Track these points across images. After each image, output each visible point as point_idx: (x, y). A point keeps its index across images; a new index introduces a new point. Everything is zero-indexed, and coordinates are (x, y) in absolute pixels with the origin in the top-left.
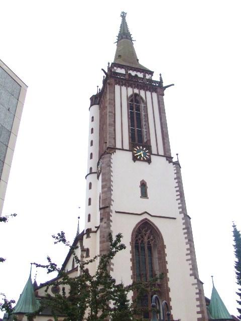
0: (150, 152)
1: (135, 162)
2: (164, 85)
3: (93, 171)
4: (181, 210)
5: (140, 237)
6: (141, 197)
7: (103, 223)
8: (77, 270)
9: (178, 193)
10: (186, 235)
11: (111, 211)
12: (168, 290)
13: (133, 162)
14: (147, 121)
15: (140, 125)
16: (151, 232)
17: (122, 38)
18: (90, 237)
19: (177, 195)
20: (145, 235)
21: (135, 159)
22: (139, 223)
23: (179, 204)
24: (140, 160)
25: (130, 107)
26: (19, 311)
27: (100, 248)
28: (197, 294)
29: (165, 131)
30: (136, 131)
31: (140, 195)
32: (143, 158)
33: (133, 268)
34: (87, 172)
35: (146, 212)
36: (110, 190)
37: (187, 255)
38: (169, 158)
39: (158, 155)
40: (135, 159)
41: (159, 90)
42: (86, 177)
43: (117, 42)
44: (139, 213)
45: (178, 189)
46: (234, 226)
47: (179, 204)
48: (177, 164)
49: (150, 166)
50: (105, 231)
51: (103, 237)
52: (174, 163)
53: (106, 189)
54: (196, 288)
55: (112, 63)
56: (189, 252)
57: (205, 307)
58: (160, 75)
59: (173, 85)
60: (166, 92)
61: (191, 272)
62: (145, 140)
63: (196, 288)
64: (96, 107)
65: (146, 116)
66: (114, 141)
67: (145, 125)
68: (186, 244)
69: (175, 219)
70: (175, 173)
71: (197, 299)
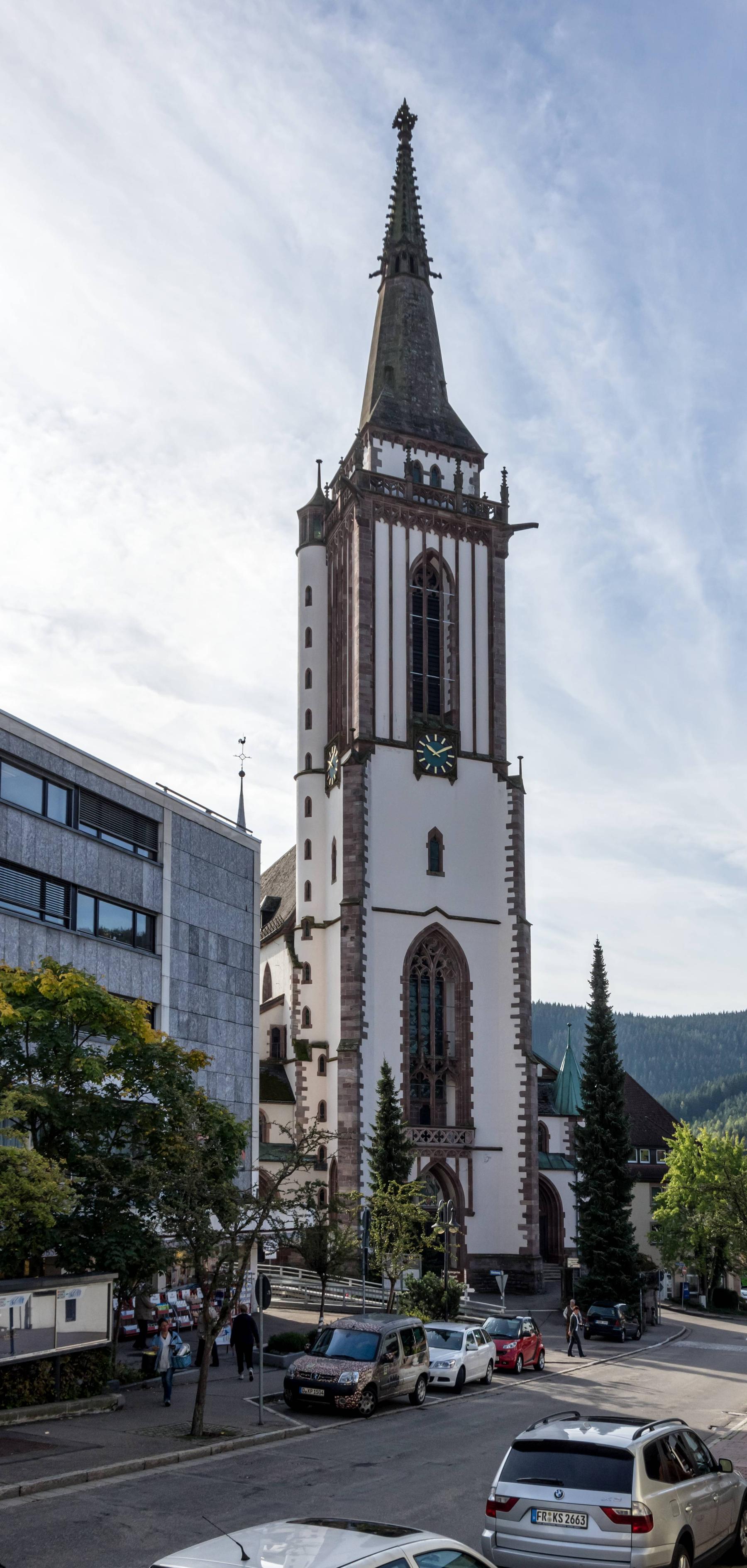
0: (457, 752)
1: (418, 778)
2: (512, 520)
4: (512, 906)
9: (511, 864)
10: (516, 965)
14: (455, 649)
15: (435, 666)
16: (445, 950)
19: (508, 869)
20: (432, 957)
21: (419, 770)
22: (420, 934)
23: (510, 890)
24: (430, 773)
25: (415, 602)
27: (342, 1012)
28: (522, 1083)
29: (497, 683)
33: (404, 1031)
35: (436, 909)
36: (363, 859)
37: (514, 1005)
38: (499, 765)
40: (419, 770)
43: (381, 272)
45: (511, 853)
47: (510, 890)
48: (516, 785)
50: (353, 957)
51: (349, 970)
54: (523, 1074)
56: (517, 1000)
57: (535, 1137)
58: (504, 473)
59: (536, 525)
60: (515, 543)
61: (515, 944)
62: (447, 708)
63: (523, 1074)
65: (455, 630)
66: (371, 717)
67: (449, 660)
68: (515, 983)
70: (510, 812)
71: (522, 1094)
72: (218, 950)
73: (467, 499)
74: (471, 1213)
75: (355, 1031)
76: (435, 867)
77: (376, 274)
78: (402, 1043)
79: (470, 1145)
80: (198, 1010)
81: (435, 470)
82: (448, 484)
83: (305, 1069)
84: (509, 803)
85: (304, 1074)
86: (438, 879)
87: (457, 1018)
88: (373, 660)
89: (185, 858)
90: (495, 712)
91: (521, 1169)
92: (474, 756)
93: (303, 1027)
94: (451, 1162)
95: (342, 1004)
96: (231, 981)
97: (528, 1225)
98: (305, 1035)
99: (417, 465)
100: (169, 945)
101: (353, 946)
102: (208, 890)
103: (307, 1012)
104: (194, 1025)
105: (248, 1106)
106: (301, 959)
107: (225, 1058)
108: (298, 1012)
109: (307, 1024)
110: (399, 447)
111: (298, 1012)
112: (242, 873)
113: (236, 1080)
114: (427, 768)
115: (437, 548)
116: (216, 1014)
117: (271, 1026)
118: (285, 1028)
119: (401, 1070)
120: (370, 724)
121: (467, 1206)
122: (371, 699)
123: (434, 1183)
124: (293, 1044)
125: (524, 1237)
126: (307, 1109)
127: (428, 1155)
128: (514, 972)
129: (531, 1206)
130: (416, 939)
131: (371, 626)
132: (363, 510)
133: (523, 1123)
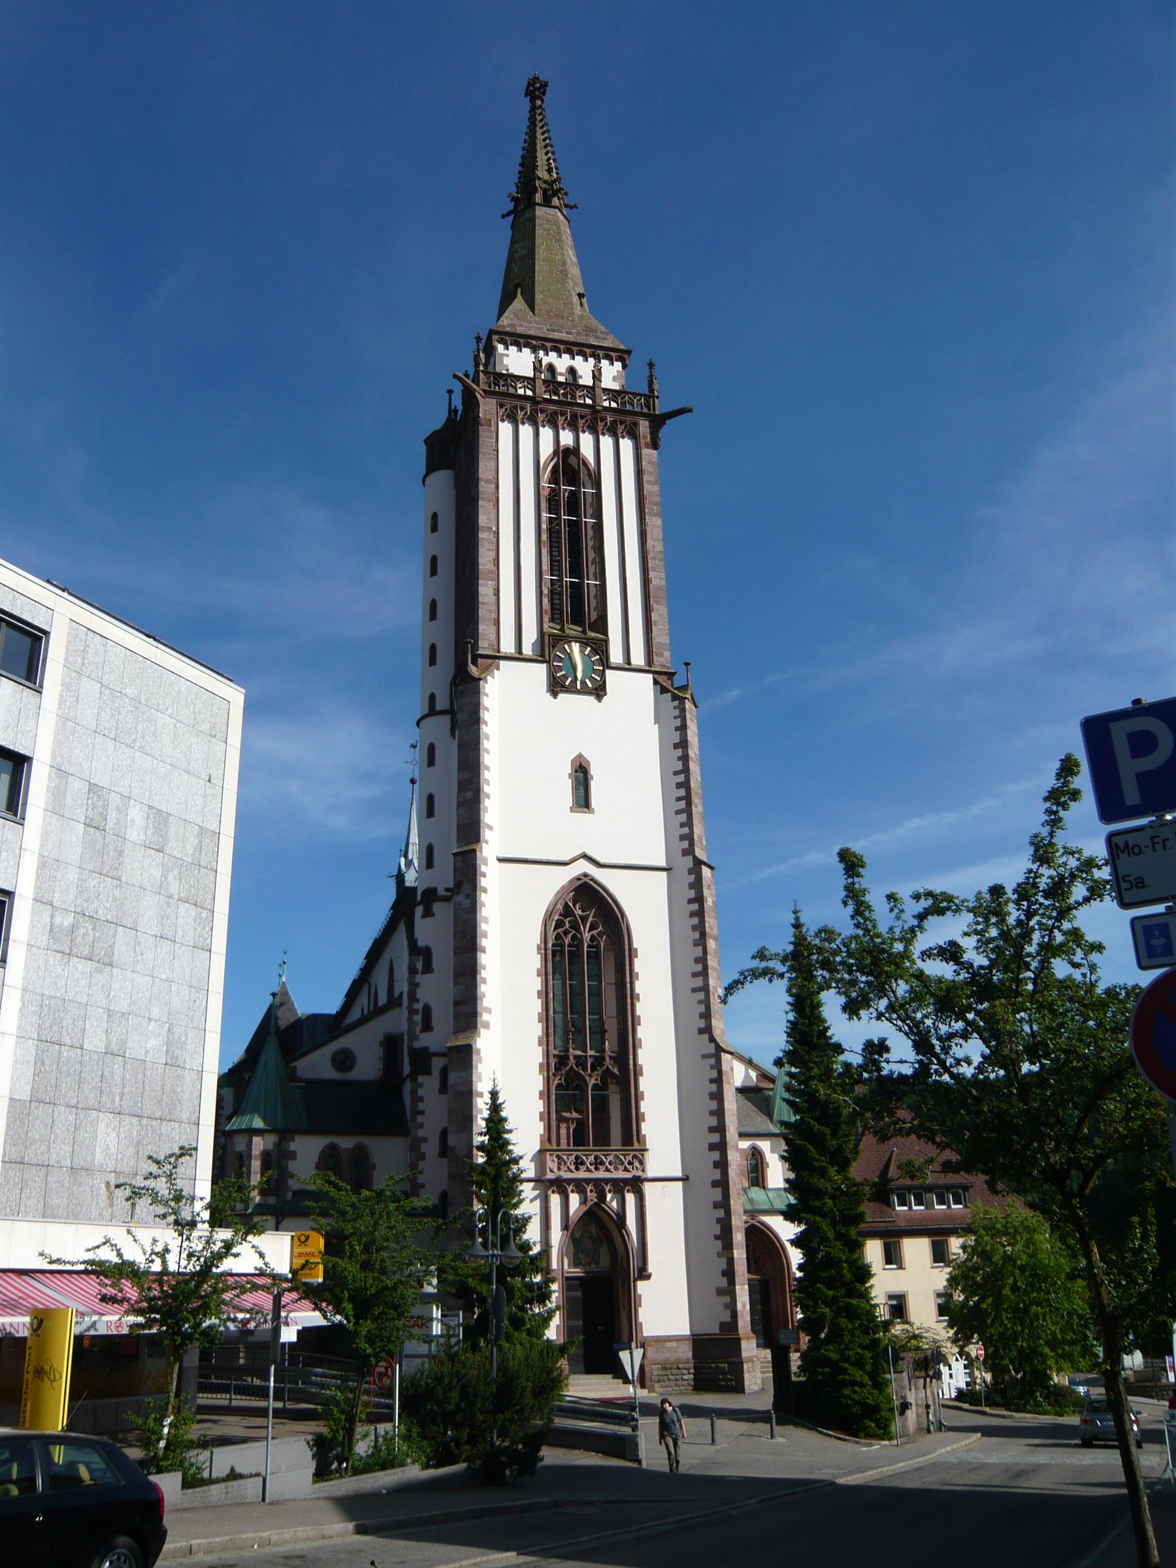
0: (605, 663)
3: (438, 707)
8: (400, 1005)
13: (548, 696)
18: (433, 915)
19: (678, 799)
21: (556, 686)
23: (682, 825)
24: (571, 690)
30: (280, 1405)
32: (583, 683)
34: (418, 707)
35: (585, 856)
40: (556, 686)
42: (418, 723)
46: (795, 912)
47: (682, 825)
58: (651, 365)
59: (690, 411)
66: (494, 628)
72: (146, 828)
76: (583, 800)
77: (508, 214)
80: (97, 912)
81: (572, 371)
82: (586, 380)
83: (421, 1085)
84: (675, 718)
85: (421, 1092)
88: (498, 566)
89: (88, 688)
92: (627, 666)
93: (423, 1030)
95: (456, 983)
96: (170, 877)
98: (425, 1040)
99: (551, 368)
100: (43, 805)
102: (135, 741)
103: (427, 1009)
104: (86, 934)
105: (194, 1075)
106: (421, 943)
107: (148, 995)
108: (416, 1012)
109: (427, 1026)
110: (526, 351)
111: (416, 1012)
112: (205, 727)
113: (170, 1030)
114: (567, 683)
116: (135, 922)
118: (402, 1036)
120: (493, 636)
122: (494, 608)
124: (410, 1055)
126: (424, 1140)
130: (556, 895)
131: (494, 529)
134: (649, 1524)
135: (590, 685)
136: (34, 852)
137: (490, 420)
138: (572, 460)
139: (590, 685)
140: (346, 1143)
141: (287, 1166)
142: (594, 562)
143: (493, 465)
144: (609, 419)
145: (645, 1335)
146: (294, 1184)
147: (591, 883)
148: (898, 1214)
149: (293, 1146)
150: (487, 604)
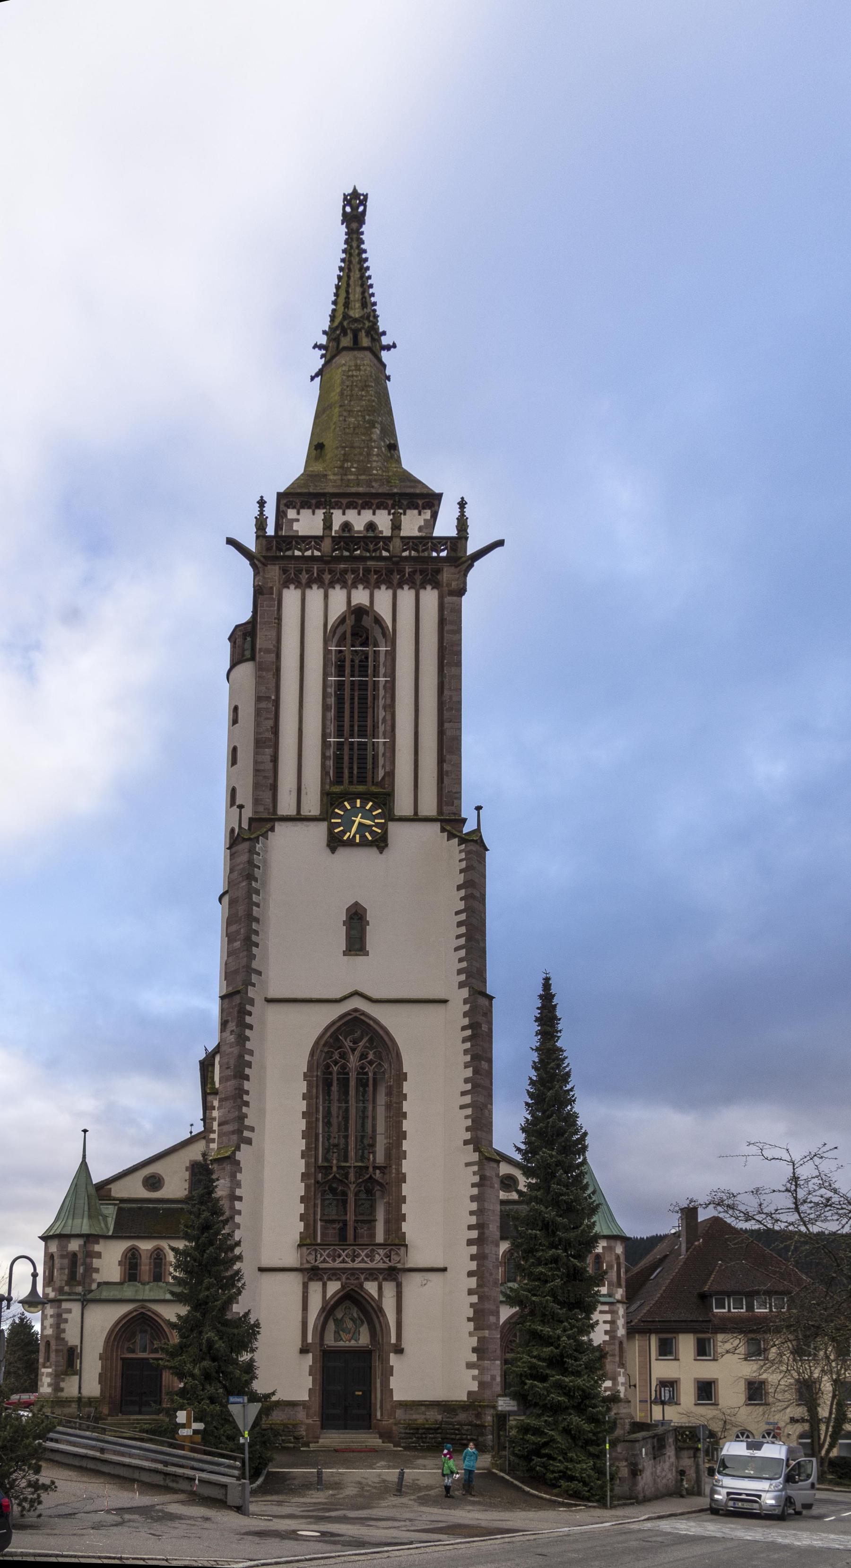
0: (390, 816)
5: (336, 1056)
6: (345, 954)
7: (227, 1034)
11: (252, 1002)
12: (402, 1178)
14: (391, 708)
17: (338, 351)
21: (335, 842)
26: (58, 1232)
29: (448, 733)
31: (341, 943)
33: (309, 1134)
35: (356, 993)
39: (416, 818)
40: (335, 842)
41: (447, 574)
43: (320, 373)
44: (339, 996)
47: (461, 960)
49: (381, 856)
51: (228, 1068)
52: (463, 840)
53: (237, 944)
54: (474, 1173)
55: (280, 496)
59: (500, 543)
63: (474, 1173)
64: (246, 669)
68: (466, 1067)
69: (445, 1001)
70: (461, 871)
71: (473, 1199)
73: (407, 541)
74: (399, 1350)
75: (232, 1136)
78: (304, 1148)
79: (399, 1266)
81: (371, 526)
86: (360, 960)
87: (386, 1117)
90: (445, 766)
91: (470, 1292)
94: (371, 1288)
97: (480, 1363)
101: (233, 1040)
115: (368, 604)
117: (190, 1161)
119: (302, 1181)
121: (393, 1340)
122: (271, 774)
123: (355, 1315)
125: (474, 1378)
127: (338, 1279)
128: (465, 1054)
129: (484, 1337)
131: (273, 697)
132: (264, 578)
133: (474, 1234)
134: (546, 1531)
135: (370, 838)
136: (191, 1133)
137: (272, 588)
138: (367, 621)
139: (370, 838)
140: (146, 1246)
141: (92, 1263)
142: (384, 720)
143: (274, 633)
144: (408, 570)
145: (398, 1396)
146: (98, 1277)
147: (362, 1017)
148: (714, 1315)
149: (97, 1248)
150: (263, 770)
